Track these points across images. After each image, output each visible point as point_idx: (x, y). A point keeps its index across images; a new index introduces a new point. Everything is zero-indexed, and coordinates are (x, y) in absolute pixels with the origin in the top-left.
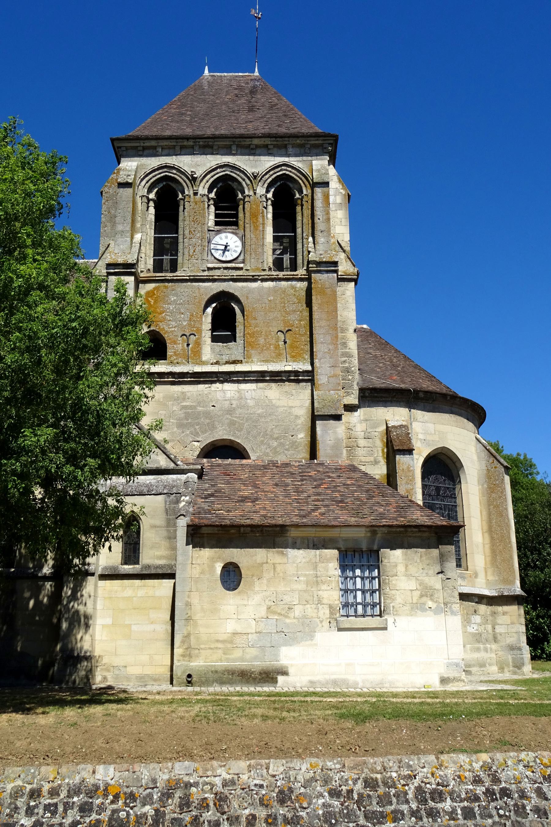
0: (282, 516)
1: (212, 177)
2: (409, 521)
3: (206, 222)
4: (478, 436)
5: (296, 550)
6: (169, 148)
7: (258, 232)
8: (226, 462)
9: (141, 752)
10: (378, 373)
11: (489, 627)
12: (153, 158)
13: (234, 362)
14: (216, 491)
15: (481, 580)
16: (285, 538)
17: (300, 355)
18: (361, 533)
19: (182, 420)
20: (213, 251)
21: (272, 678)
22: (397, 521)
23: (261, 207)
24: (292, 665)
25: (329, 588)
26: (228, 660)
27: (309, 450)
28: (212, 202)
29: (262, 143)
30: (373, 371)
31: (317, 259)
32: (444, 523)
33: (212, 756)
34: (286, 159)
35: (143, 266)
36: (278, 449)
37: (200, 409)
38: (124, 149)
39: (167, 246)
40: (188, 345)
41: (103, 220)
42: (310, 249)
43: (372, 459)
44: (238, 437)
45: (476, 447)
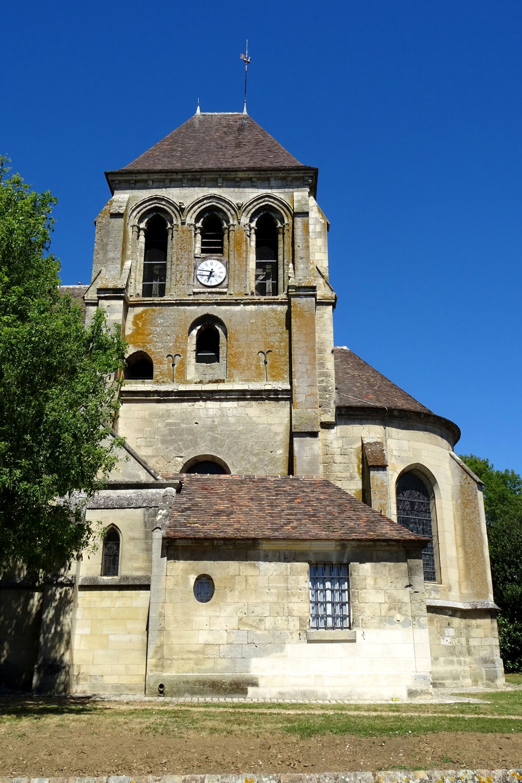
0: (255, 530)
1: (199, 208)
2: (378, 536)
3: (193, 250)
4: (452, 453)
5: (267, 563)
6: (160, 181)
7: (241, 259)
8: (205, 477)
9: (81, 764)
10: (354, 392)
11: (463, 640)
12: (144, 191)
13: (217, 381)
14: (193, 505)
15: (455, 593)
16: (257, 551)
17: (280, 375)
18: (331, 547)
19: (166, 436)
20: (199, 277)
21: (243, 689)
22: (367, 534)
23: (245, 236)
24: (262, 677)
25: (299, 600)
26: (199, 671)
27: (287, 465)
28: (198, 231)
29: (246, 176)
30: (349, 390)
31: (297, 284)
32: (413, 538)
33: (150, 770)
34: (269, 191)
35: (132, 291)
36: (258, 465)
37: (183, 426)
38: (118, 182)
39: (157, 272)
40: (173, 365)
41: (96, 248)
42: (290, 275)
43: (348, 474)
44: (219, 453)
45: (450, 464)
